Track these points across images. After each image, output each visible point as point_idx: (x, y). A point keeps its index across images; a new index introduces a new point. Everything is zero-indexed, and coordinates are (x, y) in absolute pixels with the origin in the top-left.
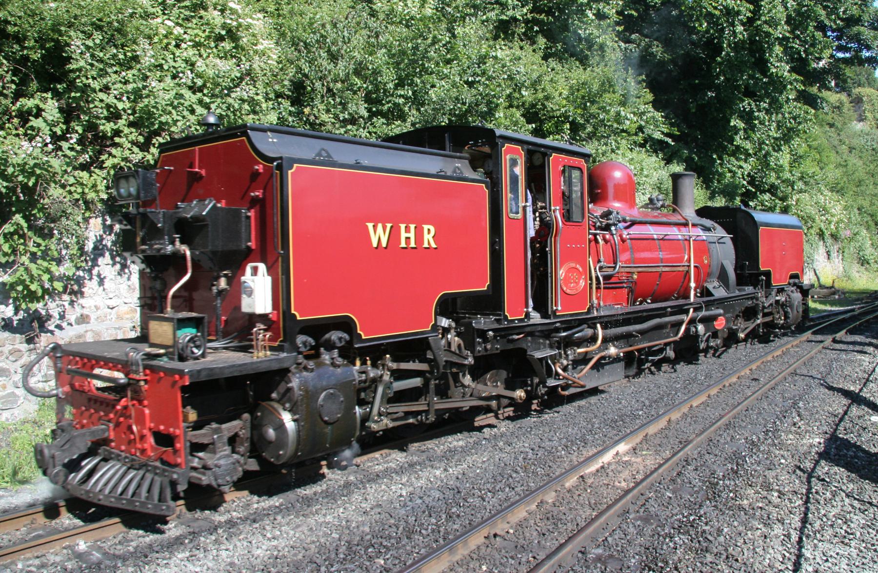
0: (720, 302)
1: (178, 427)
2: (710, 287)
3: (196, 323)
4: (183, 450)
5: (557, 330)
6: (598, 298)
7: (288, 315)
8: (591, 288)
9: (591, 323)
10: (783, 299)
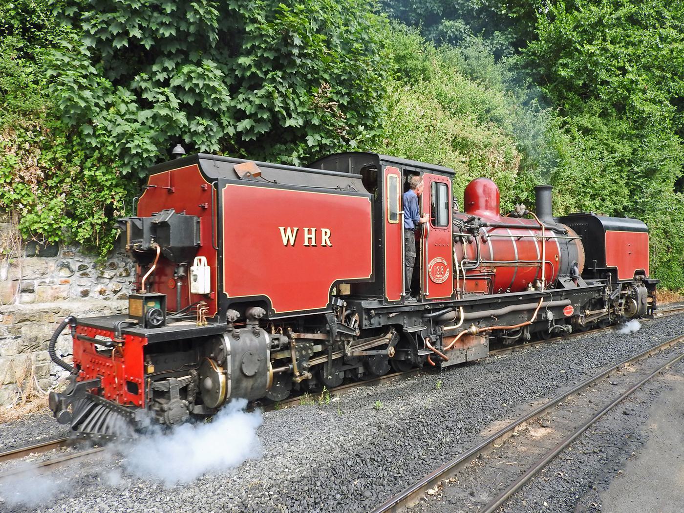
0: (569, 294)
1: (140, 378)
2: (562, 280)
3: (160, 300)
4: (143, 393)
5: (429, 311)
6: (461, 287)
7: (221, 295)
8: (455, 279)
9: (455, 306)
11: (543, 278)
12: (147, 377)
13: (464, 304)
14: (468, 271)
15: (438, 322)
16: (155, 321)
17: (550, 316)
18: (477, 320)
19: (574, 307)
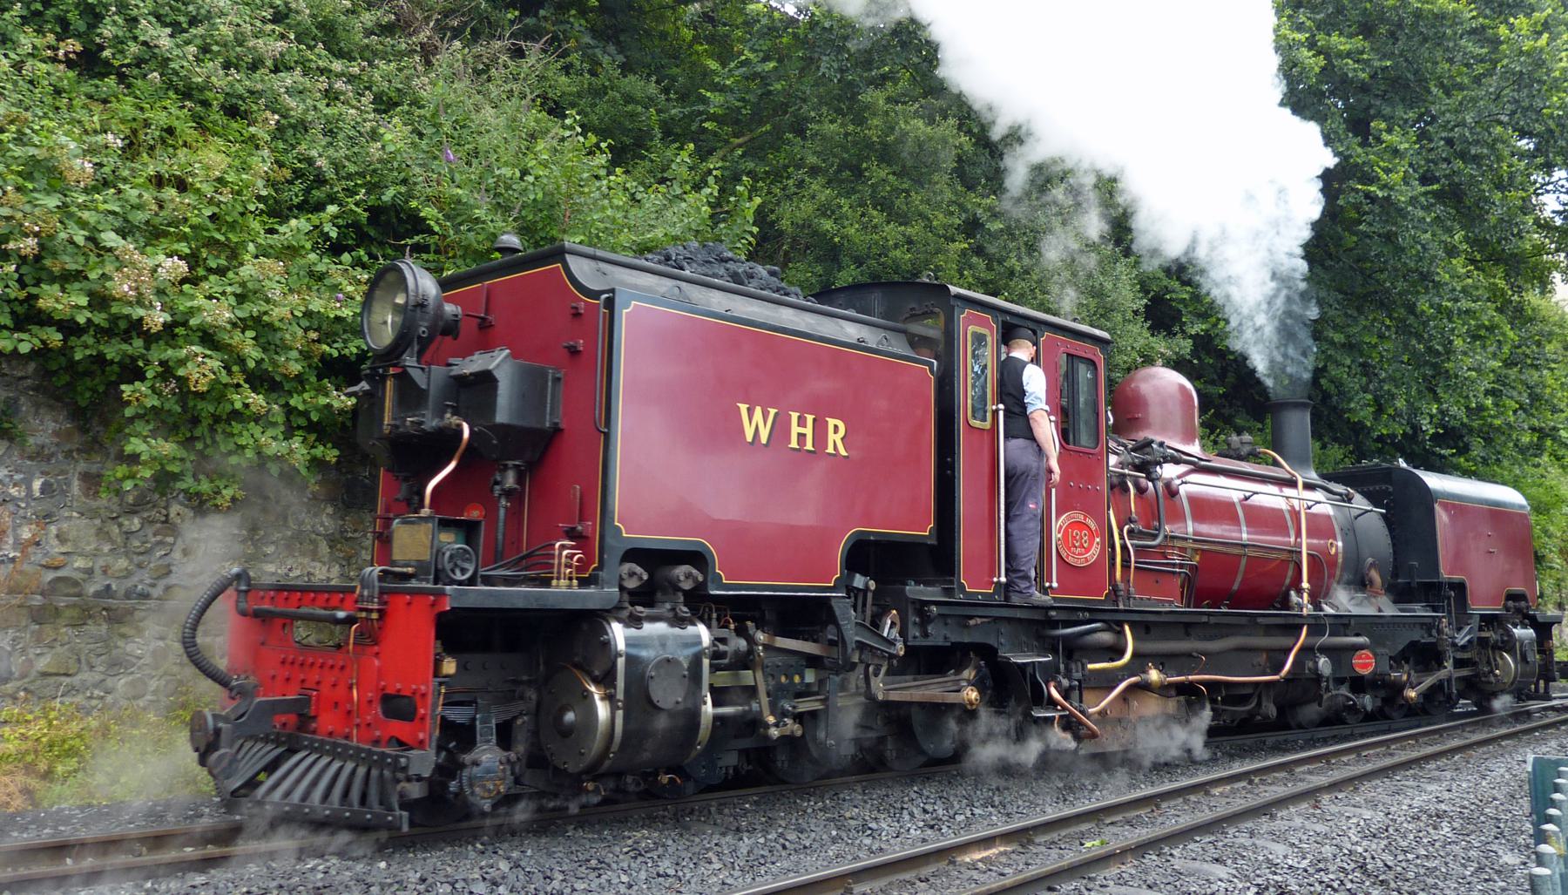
11: (1305, 585)
12: (441, 684)
13: (1136, 617)
14: (1140, 550)
15: (1074, 650)
16: (458, 572)
17: (1323, 663)
19: (1375, 655)
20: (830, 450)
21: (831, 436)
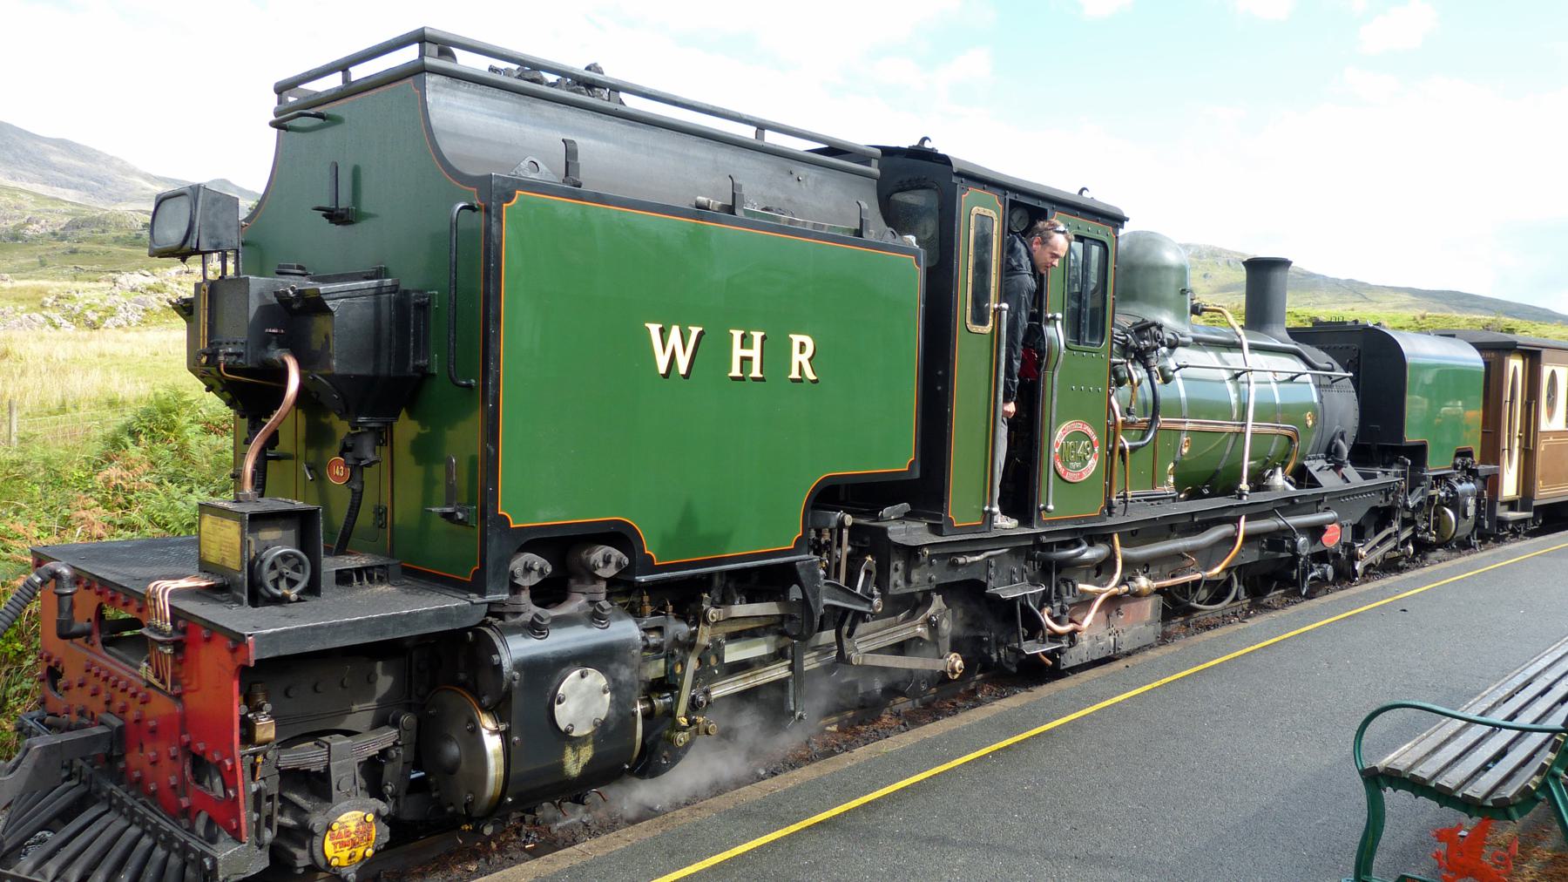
10: (1442, 494)
18: (1146, 565)
20: (795, 374)
21: (797, 357)
